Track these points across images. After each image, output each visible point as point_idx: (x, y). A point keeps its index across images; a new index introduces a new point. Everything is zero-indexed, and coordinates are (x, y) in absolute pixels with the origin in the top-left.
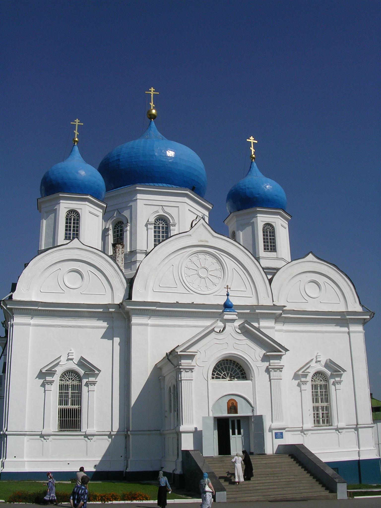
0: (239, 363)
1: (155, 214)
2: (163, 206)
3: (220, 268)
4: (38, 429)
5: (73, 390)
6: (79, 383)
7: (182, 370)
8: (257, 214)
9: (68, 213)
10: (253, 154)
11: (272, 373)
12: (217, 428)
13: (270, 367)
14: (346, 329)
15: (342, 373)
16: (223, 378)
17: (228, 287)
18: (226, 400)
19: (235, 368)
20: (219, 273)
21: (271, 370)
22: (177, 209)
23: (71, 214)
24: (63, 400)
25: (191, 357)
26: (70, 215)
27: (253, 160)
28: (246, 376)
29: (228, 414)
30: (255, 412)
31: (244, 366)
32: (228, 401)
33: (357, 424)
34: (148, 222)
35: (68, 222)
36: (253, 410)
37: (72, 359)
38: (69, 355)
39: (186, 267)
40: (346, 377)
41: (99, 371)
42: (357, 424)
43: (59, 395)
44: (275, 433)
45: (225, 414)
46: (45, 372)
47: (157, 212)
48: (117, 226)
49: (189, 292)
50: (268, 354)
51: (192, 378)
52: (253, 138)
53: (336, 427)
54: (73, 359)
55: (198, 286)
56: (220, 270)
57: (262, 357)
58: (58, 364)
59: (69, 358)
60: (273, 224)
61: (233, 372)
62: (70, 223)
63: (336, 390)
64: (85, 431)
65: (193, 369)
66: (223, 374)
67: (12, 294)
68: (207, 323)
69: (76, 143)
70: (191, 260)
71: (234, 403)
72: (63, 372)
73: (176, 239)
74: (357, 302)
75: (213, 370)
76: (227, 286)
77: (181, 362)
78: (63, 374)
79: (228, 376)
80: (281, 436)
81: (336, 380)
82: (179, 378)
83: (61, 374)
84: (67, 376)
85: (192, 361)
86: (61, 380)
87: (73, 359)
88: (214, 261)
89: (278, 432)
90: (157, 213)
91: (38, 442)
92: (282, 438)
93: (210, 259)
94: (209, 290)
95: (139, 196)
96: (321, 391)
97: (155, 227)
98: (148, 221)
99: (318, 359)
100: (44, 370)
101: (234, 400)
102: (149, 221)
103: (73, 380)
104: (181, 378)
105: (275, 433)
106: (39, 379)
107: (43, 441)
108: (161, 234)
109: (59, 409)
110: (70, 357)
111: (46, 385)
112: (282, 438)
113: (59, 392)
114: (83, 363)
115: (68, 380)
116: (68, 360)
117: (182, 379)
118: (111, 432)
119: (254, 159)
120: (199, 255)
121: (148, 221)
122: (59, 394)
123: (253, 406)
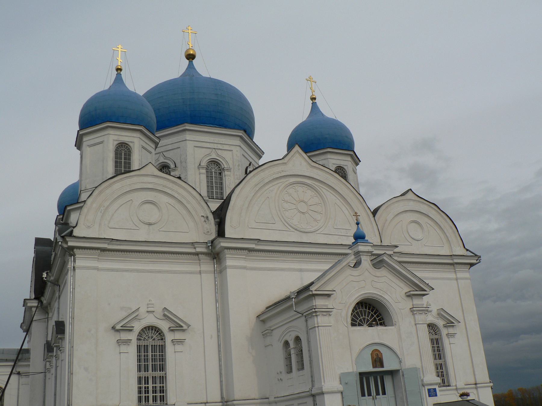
2: (216, 149)
7: (318, 314)
9: (117, 147)
14: (453, 276)
18: (369, 352)
19: (371, 313)
22: (230, 152)
28: (384, 322)
29: (373, 368)
30: (403, 364)
34: (199, 166)
35: (119, 155)
40: (459, 330)
41: (189, 326)
43: (138, 359)
44: (428, 389)
45: (370, 368)
47: (209, 155)
49: (290, 229)
53: (455, 387)
56: (321, 205)
58: (135, 318)
67: (73, 230)
70: (288, 191)
71: (379, 354)
73: (270, 166)
75: (353, 309)
78: (151, 327)
79: (366, 324)
80: (434, 393)
82: (315, 324)
84: (152, 333)
86: (140, 340)
89: (431, 389)
90: (208, 156)
96: (438, 345)
102: (201, 165)
103: (154, 340)
104: (318, 324)
105: (428, 389)
110: (150, 309)
112: (436, 395)
113: (138, 355)
114: (167, 315)
117: (319, 325)
120: (288, 191)
121: (200, 165)
122: (138, 357)
123: (400, 357)
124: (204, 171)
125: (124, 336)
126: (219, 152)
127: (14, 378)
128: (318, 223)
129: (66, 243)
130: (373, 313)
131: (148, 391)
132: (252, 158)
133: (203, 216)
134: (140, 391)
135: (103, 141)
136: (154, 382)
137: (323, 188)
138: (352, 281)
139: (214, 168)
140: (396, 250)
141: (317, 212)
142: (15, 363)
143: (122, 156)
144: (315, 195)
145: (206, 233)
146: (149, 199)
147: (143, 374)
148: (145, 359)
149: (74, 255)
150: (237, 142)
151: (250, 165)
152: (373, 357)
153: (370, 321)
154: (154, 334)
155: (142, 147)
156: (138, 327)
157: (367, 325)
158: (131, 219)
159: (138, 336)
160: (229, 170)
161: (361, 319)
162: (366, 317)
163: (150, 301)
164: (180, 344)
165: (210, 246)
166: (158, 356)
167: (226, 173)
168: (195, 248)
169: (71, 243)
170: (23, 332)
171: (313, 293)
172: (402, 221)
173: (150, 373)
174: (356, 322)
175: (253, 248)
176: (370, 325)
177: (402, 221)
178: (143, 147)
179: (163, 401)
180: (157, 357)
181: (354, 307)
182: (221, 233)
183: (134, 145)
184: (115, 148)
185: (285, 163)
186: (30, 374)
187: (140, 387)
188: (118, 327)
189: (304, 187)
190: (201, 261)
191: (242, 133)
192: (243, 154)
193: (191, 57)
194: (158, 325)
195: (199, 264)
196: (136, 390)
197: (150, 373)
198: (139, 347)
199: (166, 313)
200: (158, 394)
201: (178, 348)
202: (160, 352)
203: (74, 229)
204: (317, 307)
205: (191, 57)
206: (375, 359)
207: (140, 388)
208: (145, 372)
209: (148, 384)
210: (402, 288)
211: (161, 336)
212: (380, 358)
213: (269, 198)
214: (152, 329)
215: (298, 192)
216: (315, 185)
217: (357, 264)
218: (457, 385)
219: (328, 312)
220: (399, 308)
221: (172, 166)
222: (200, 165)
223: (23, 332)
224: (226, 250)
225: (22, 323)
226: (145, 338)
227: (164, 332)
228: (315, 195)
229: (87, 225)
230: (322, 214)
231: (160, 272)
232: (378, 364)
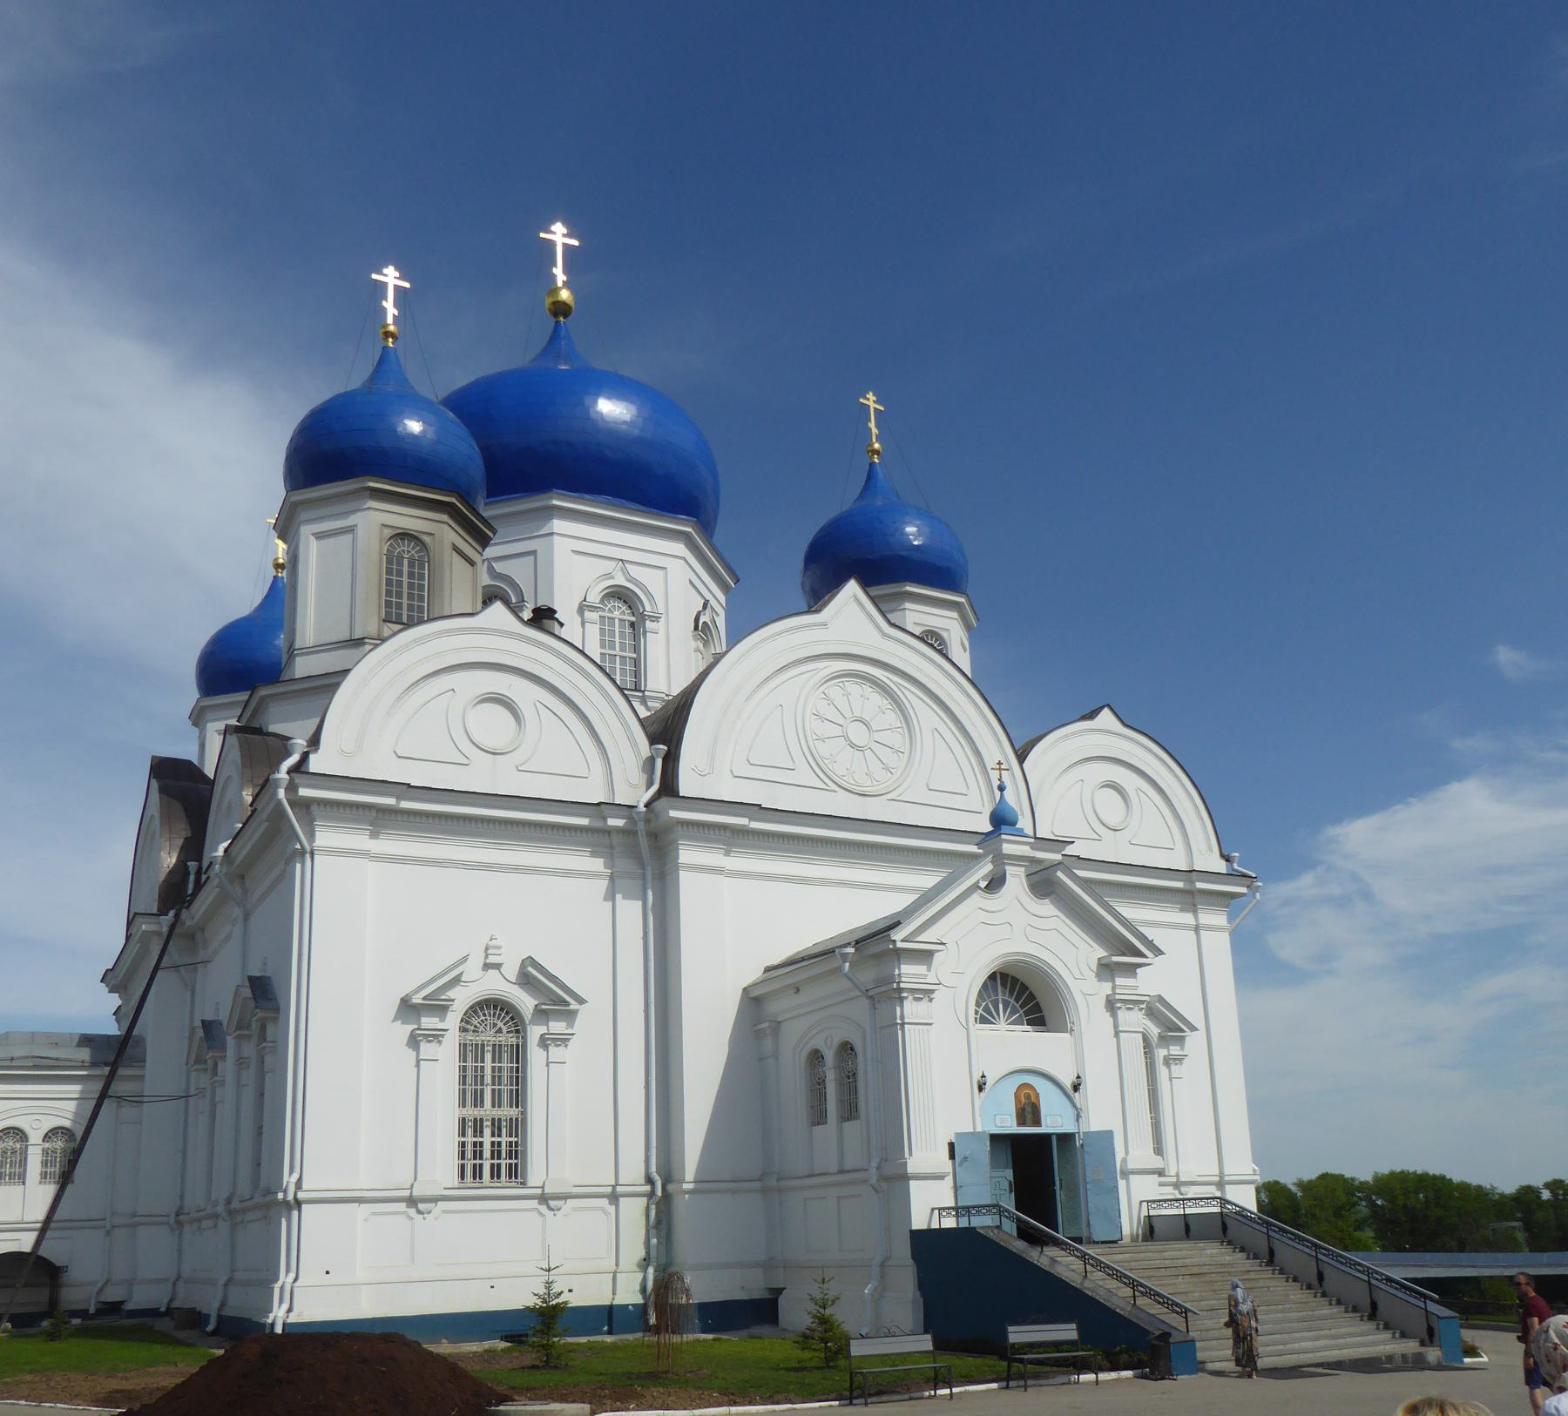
1: (603, 580)
3: (900, 725)
4: (400, 1177)
5: (476, 1062)
6: (518, 1038)
7: (905, 995)
8: (903, 604)
10: (874, 440)
11: (1122, 1014)
12: (1011, 1164)
14: (1188, 918)
15: (1188, 1033)
17: (1002, 767)
20: (898, 740)
21: (1119, 1005)
22: (661, 572)
24: (470, 1093)
25: (925, 956)
27: (876, 456)
31: (1041, 997)
32: (1017, 1089)
33: (1221, 1175)
34: (584, 603)
36: (1078, 1117)
37: (497, 966)
38: (489, 952)
39: (814, 714)
42: (1221, 1175)
45: (1009, 1125)
46: (420, 1001)
47: (609, 576)
50: (1116, 959)
51: (932, 1018)
53: (1175, 1179)
54: (501, 965)
55: (848, 769)
57: (1095, 970)
59: (488, 961)
60: (945, 634)
62: (399, 595)
63: (1170, 1080)
64: (541, 1185)
65: (932, 991)
69: (390, 340)
72: (469, 1006)
74: (1213, 847)
76: (1000, 763)
77: (899, 970)
81: (1172, 1053)
82: (896, 1019)
83: (463, 1013)
85: (929, 970)
87: (501, 965)
88: (885, 703)
91: (398, 1221)
93: (876, 699)
94: (876, 783)
95: (558, 525)
98: (585, 600)
100: (416, 996)
101: (1022, 1084)
104: (902, 1017)
106: (402, 1023)
107: (412, 1218)
110: (492, 959)
111: (421, 1044)
116: (487, 966)
117: (906, 1021)
118: (614, 1187)
119: (878, 455)
121: (585, 600)
123: (1078, 1106)
128: (892, 773)
132: (711, 592)
136: (496, 1131)
137: (908, 689)
140: (1069, 850)
143: (402, 566)
147: (471, 1112)
150: (679, 548)
151: (705, 606)
152: (1020, 1102)
155: (454, 549)
156: (463, 999)
164: (560, 1045)
170: (110, 992)
172: (1082, 780)
177: (1082, 780)
182: (669, 787)
183: (434, 539)
185: (825, 624)
186: (146, 1099)
188: (417, 999)
191: (693, 529)
194: (510, 996)
197: (487, 1111)
198: (463, 1047)
207: (463, 1145)
208: (511, 1107)
212: (1033, 1103)
214: (495, 1008)
215: (866, 701)
216: (891, 680)
217: (995, 883)
218: (1181, 1174)
225: (107, 970)
232: (1029, 1117)
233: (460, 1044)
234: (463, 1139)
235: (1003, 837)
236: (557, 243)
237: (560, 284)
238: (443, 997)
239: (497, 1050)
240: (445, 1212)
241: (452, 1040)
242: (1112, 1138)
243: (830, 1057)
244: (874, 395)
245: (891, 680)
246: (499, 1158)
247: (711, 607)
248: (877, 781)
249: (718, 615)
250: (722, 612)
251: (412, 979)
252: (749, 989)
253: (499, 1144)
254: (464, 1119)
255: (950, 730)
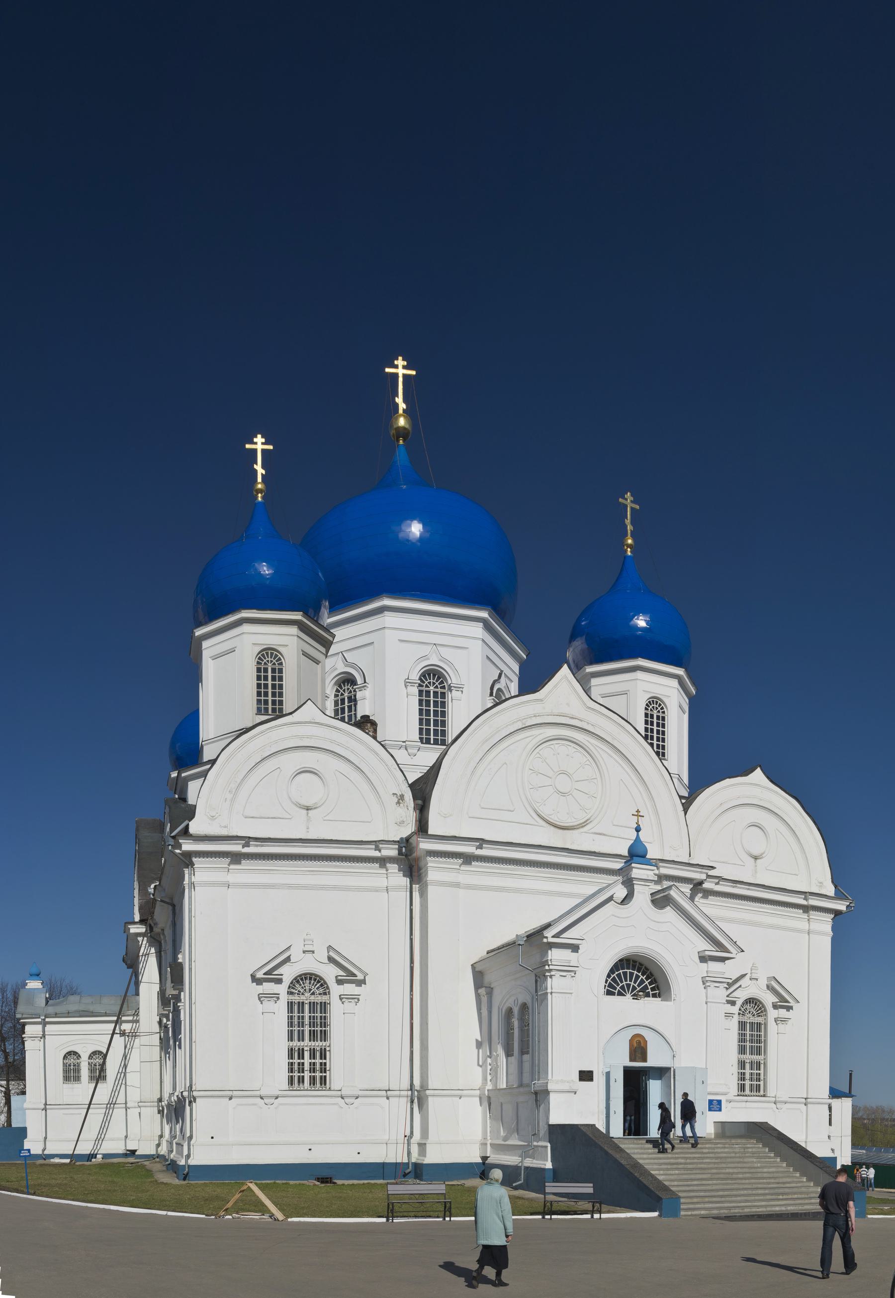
0: (649, 967)
3: (594, 777)
9: (260, 657)
13: (708, 979)
16: (620, 994)
19: (642, 977)
23: (267, 659)
26: (269, 659)
34: (407, 680)
40: (797, 1014)
43: (288, 1022)
47: (425, 657)
48: (341, 691)
52: (262, 437)
58: (288, 959)
61: (637, 984)
66: (626, 983)
68: (586, 885)
70: (541, 753)
75: (608, 973)
80: (718, 1106)
82: (547, 989)
84: (310, 983)
86: (292, 993)
89: (714, 1100)
92: (720, 1110)
95: (389, 619)
97: (421, 692)
99: (754, 976)
100: (259, 973)
103: (313, 994)
106: (572, 952)
108: (432, 708)
109: (288, 1049)
110: (307, 948)
112: (720, 1110)
113: (288, 1016)
115: (303, 994)
123: (674, 1050)
124: (415, 690)
125: (269, 987)
126: (444, 652)
127: (118, 1040)
128: (586, 813)
129: (179, 846)
130: (644, 978)
131: (303, 1069)
133: (396, 794)
134: (292, 1069)
135: (236, 647)
138: (614, 925)
139: (434, 683)
141: (587, 794)
142: (118, 1018)
144: (588, 763)
145: (398, 823)
146: (307, 766)
147: (296, 1044)
148: (299, 1022)
149: (192, 864)
153: (637, 989)
154: (313, 985)
156: (288, 973)
157: (631, 996)
158: (279, 802)
159: (289, 987)
160: (460, 688)
161: (624, 985)
162: (632, 983)
163: (307, 935)
165: (404, 848)
166: (319, 1018)
167: (455, 694)
168: (380, 851)
169: (187, 846)
170: (128, 968)
171: (549, 941)
173: (307, 1044)
174: (615, 989)
175: (473, 853)
176: (636, 997)
178: (305, 654)
179: (325, 1084)
180: (317, 1020)
181: (610, 971)
182: (422, 827)
184: (257, 660)
185: (541, 700)
187: (292, 1063)
188: (260, 975)
189: (571, 746)
190: (389, 871)
192: (487, 656)
193: (638, 830)
195: (385, 876)
196: (286, 1067)
197: (307, 1044)
198: (290, 1005)
199: (332, 954)
200: (318, 1074)
201: (349, 1006)
202: (321, 1013)
203: (190, 823)
204: (553, 963)
205: (638, 830)
206: (635, 1048)
209: (303, 1058)
210: (694, 944)
211: (324, 988)
212: (642, 1047)
213: (506, 764)
216: (589, 742)
219: (570, 971)
220: (684, 975)
221: (359, 681)
222: (408, 679)
223: (128, 968)
224: (429, 859)
226: (299, 991)
227: (328, 983)
228: (588, 763)
229: (210, 815)
230: (595, 797)
231: (323, 888)
232: (639, 1055)
233: (288, 1002)
234: (291, 1061)
235: (633, 865)
236: (258, 472)
237: (401, 411)
238: (274, 973)
239: (312, 1005)
240: (787, 1109)
241: (284, 998)
242: (584, 1072)
243: (516, 1011)
244: (632, 495)
245: (589, 742)
246: (299, 1077)
247: (505, 674)
248: (575, 819)
249: (511, 681)
250: (516, 680)
251: (258, 960)
252: (54, 1016)
253: (314, 1064)
254: (292, 1049)
255: (632, 780)
